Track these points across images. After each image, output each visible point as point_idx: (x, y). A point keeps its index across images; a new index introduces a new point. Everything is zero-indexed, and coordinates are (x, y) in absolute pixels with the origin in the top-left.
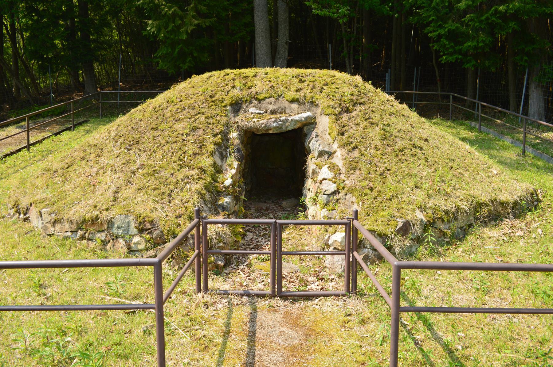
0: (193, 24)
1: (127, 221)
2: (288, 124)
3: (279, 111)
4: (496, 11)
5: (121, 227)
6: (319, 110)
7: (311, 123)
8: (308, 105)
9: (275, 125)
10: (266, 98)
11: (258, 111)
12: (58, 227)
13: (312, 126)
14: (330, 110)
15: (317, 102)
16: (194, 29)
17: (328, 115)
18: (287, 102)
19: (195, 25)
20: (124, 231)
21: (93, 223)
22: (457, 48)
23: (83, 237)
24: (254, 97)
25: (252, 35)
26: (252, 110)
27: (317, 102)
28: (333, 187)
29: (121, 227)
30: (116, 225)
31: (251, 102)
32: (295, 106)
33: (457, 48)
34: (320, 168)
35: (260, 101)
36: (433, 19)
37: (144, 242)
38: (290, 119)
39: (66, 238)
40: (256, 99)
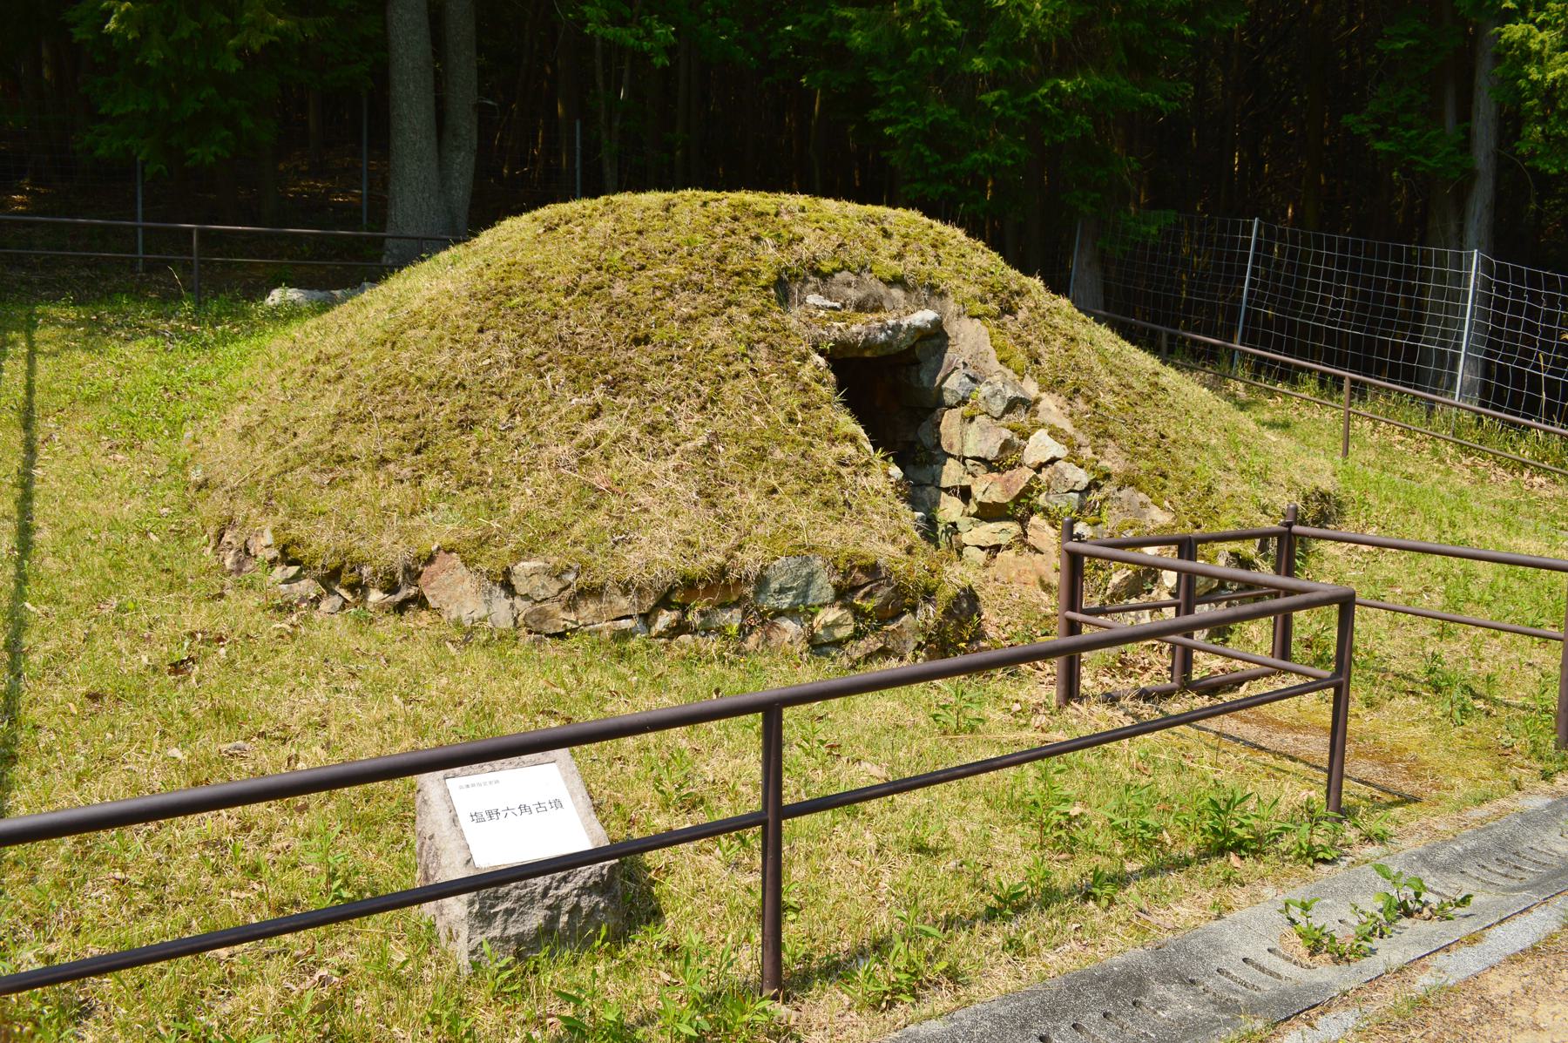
0: (272, 28)
1: (805, 571)
2: (902, 336)
3: (870, 304)
4: (1056, 90)
5: (790, 589)
6: (952, 307)
7: (935, 338)
8: (924, 293)
9: (882, 336)
10: (835, 270)
11: (828, 303)
12: (588, 609)
13: (937, 341)
14: (979, 308)
15: (942, 287)
16: (271, 43)
17: (978, 317)
18: (881, 285)
19: (276, 33)
20: (796, 597)
21: (709, 589)
22: (945, 168)
23: (679, 628)
24: (811, 268)
25: (382, 76)
26: (813, 299)
27: (942, 287)
28: (1082, 478)
29: (790, 589)
30: (774, 585)
31: (806, 281)
32: (897, 293)
33: (945, 168)
34: (1025, 436)
35: (826, 277)
36: (898, 92)
37: (850, 620)
38: (905, 323)
39: (625, 635)
40: (817, 273)
